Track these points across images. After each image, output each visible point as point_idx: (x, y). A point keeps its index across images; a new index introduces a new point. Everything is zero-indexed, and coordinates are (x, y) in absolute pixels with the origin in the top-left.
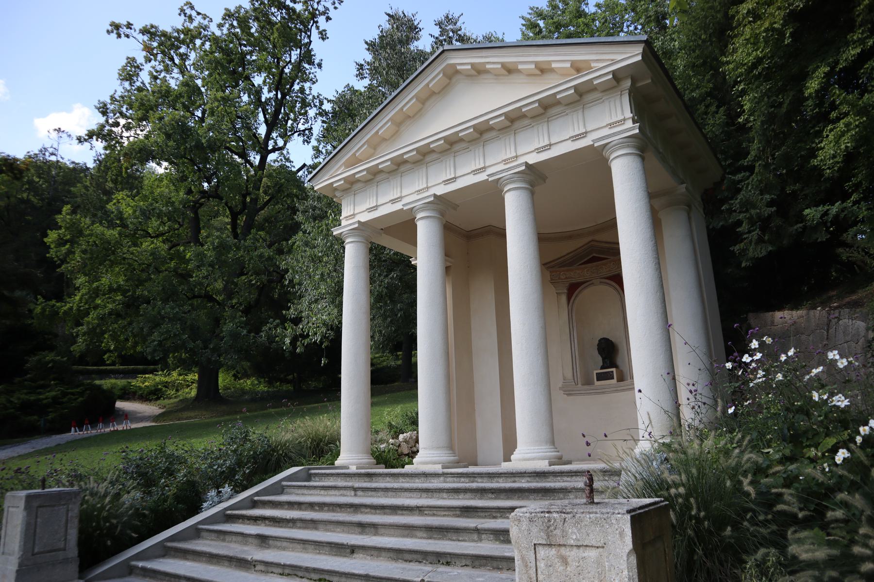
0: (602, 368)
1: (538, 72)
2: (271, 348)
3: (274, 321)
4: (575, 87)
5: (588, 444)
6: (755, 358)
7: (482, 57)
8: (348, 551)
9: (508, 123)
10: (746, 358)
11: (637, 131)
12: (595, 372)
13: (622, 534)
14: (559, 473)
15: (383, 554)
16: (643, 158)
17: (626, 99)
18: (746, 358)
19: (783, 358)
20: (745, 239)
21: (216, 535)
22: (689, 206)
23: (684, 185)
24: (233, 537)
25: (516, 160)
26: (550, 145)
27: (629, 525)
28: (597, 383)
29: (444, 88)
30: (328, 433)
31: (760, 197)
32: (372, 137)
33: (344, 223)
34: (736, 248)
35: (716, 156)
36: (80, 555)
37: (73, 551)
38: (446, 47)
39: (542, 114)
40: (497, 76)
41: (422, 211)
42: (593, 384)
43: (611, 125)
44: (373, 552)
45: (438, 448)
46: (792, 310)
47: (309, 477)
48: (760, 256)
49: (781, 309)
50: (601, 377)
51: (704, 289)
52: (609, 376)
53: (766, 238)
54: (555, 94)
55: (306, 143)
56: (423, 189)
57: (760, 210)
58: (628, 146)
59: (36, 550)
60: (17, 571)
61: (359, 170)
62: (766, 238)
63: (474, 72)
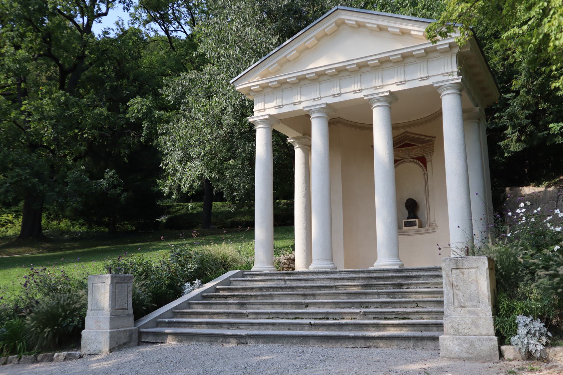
0: (408, 218)
1: (401, 34)
2: (108, 194)
3: (110, 171)
4: (425, 49)
5: (440, 249)
6: (522, 211)
7: (364, 18)
8: (304, 306)
9: (379, 64)
10: (518, 211)
11: (460, 81)
12: (404, 221)
13: (484, 263)
14: (410, 270)
15: (327, 306)
16: (461, 95)
17: (454, 59)
18: (518, 211)
19: (535, 211)
20: (508, 138)
21: (204, 306)
22: (479, 120)
23: (479, 108)
24: (218, 306)
25: (382, 88)
26: (405, 81)
27: (487, 260)
28: (405, 228)
29: (333, 33)
30: (17, 293)
31: (522, 112)
32: (281, 58)
33: (256, 114)
34: (502, 144)
35: (494, 80)
36: (134, 313)
37: (131, 311)
38: (339, 7)
39: (401, 61)
40: (372, 30)
41: (317, 113)
42: (402, 229)
43: (444, 74)
44: (320, 306)
45: (326, 260)
46: (535, 186)
47: (244, 276)
48: (518, 150)
49: (527, 185)
50: (407, 224)
51: (485, 172)
52: (413, 224)
53: (523, 138)
54: (412, 52)
55: (126, 10)
56: (317, 98)
57: (521, 121)
58: (454, 88)
59: (116, 308)
60: (110, 318)
61: (272, 80)
62: (523, 138)
63: (356, 26)
